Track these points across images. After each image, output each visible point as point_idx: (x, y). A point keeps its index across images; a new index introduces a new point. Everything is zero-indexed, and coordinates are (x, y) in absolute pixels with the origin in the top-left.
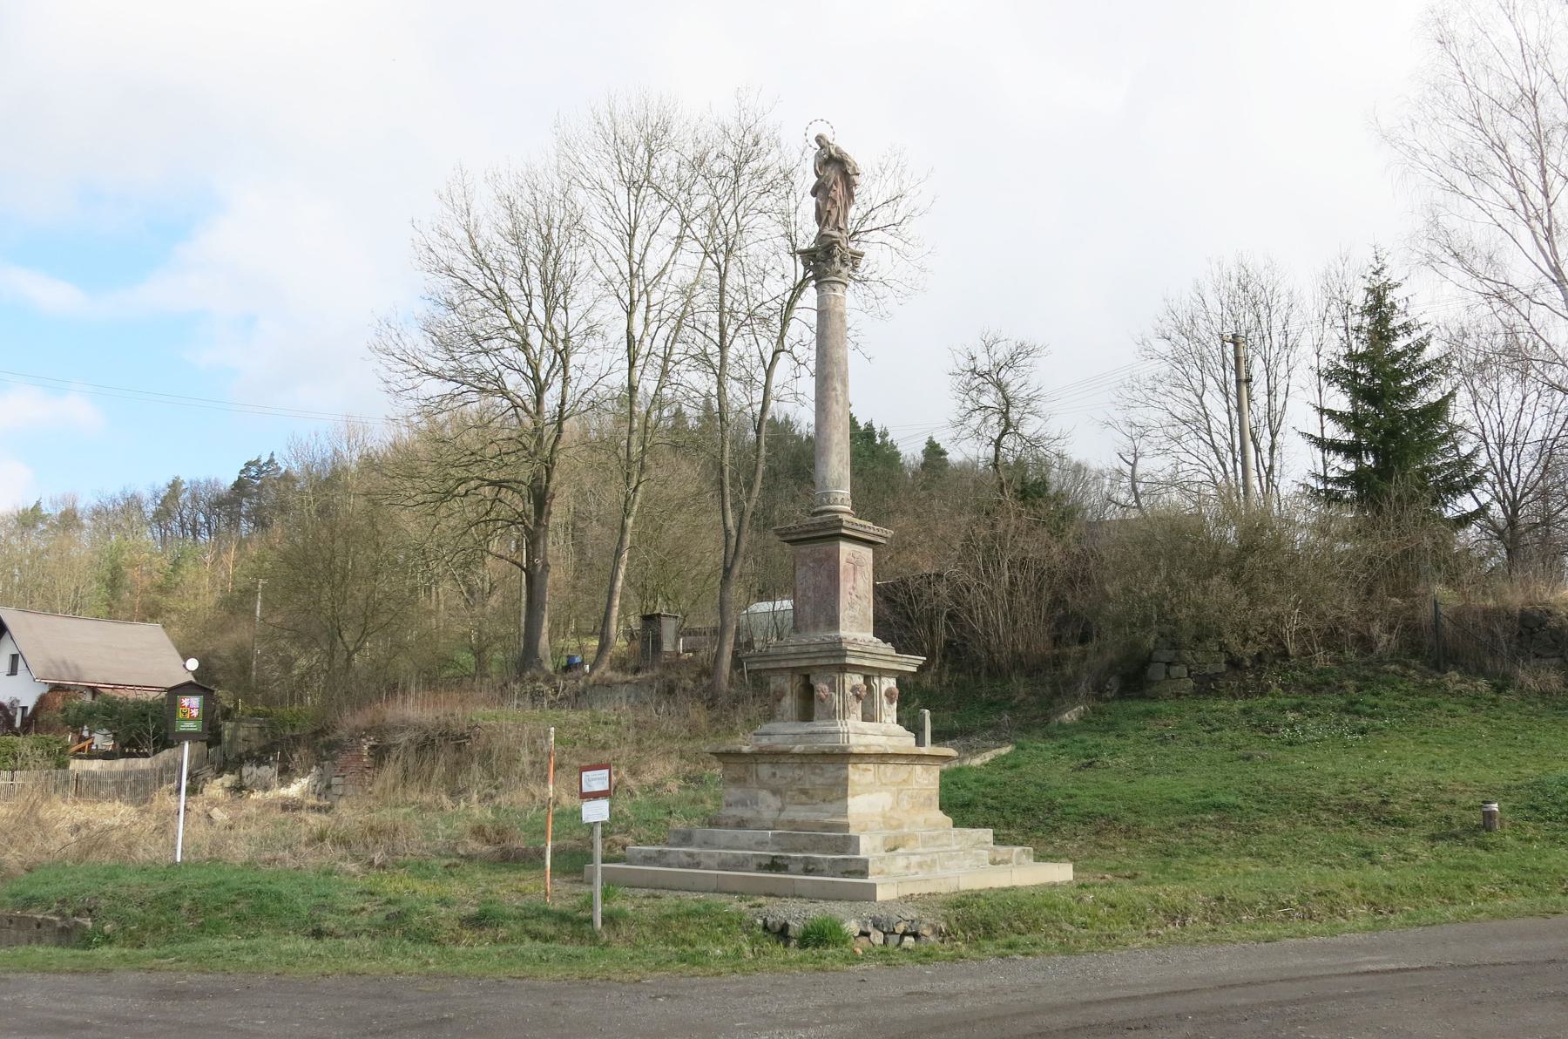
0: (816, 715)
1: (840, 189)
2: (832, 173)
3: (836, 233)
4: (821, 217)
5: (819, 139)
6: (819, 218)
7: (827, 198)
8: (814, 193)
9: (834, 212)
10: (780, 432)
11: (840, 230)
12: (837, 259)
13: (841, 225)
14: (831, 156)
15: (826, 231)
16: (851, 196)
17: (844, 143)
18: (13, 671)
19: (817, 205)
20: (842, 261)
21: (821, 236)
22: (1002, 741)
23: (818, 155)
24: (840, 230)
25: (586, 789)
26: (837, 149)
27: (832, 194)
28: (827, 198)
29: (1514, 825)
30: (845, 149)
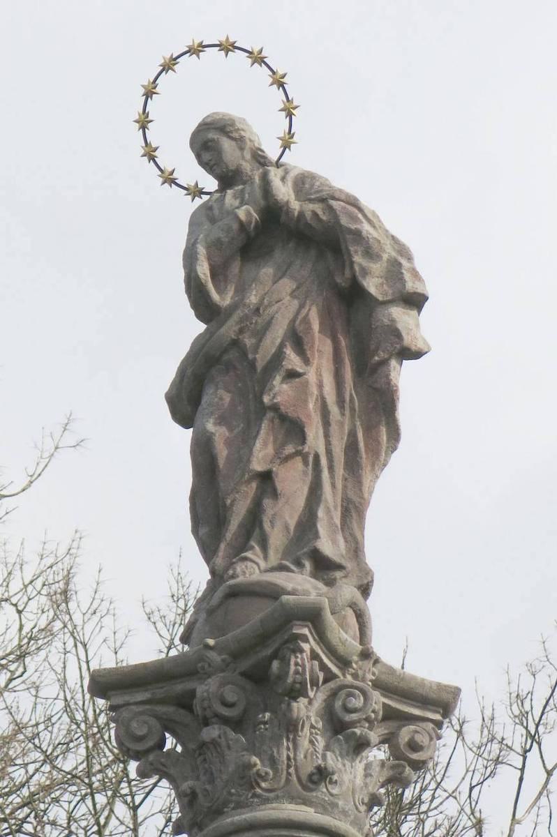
1: (319, 375)
2: (281, 295)
3: (302, 585)
5: (212, 141)
8: (185, 401)
10: (234, 340)
11: (323, 567)
12: (308, 709)
13: (330, 545)
14: (272, 213)
15: (253, 570)
16: (379, 408)
19: (203, 454)
20: (336, 725)
21: (223, 598)
22: (189, 622)
23: (205, 217)
24: (323, 567)
25: (96, 795)
26: (304, 184)
27: (280, 391)
28: (254, 410)
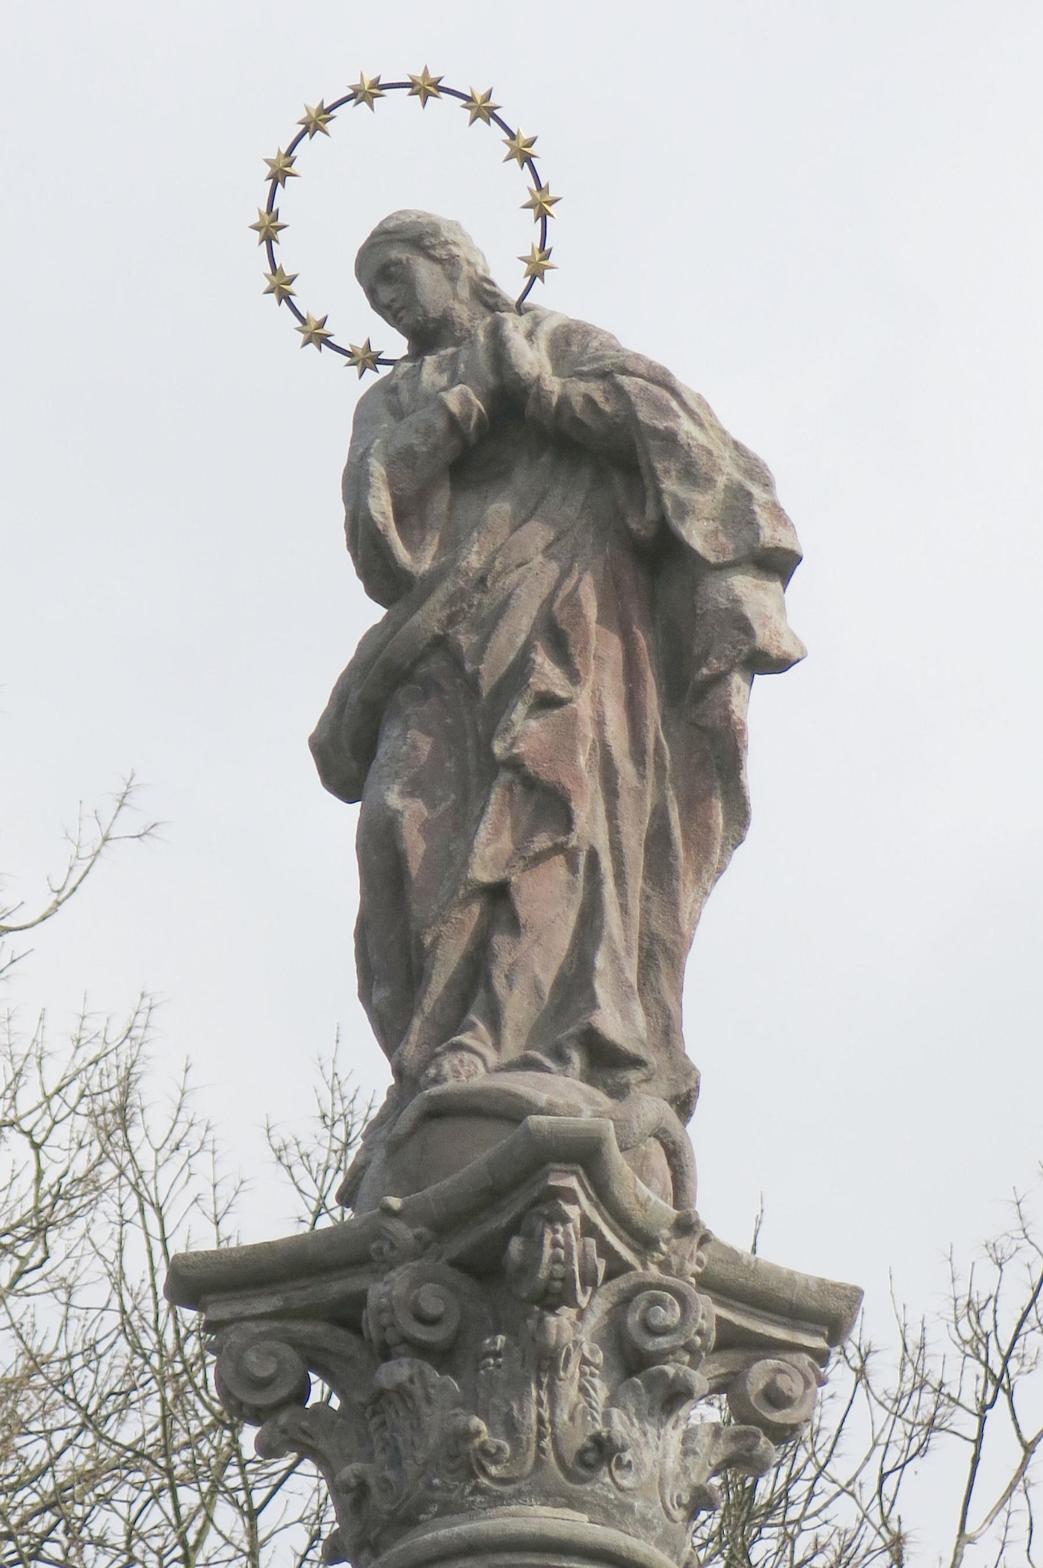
0: (785, 544)
2: (525, 553)
3: (564, 1097)
4: (410, 958)
6: (392, 963)
7: (474, 769)
8: (346, 754)
9: (548, 901)
11: (605, 1062)
12: (576, 1329)
13: (617, 1021)
14: (510, 400)
15: (473, 1067)
16: (711, 763)
17: (619, 285)
18: (899, 1517)
20: (630, 1359)
21: (419, 1120)
24: (605, 1062)
26: (569, 343)
27: (525, 733)
28: (474, 769)
29: (45, 1414)
30: (638, 331)
